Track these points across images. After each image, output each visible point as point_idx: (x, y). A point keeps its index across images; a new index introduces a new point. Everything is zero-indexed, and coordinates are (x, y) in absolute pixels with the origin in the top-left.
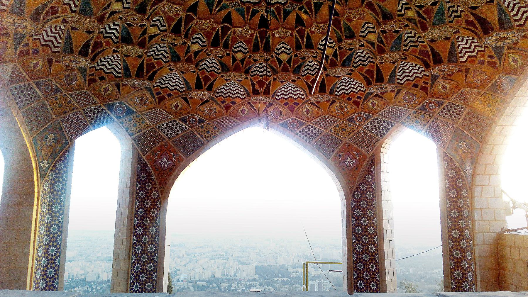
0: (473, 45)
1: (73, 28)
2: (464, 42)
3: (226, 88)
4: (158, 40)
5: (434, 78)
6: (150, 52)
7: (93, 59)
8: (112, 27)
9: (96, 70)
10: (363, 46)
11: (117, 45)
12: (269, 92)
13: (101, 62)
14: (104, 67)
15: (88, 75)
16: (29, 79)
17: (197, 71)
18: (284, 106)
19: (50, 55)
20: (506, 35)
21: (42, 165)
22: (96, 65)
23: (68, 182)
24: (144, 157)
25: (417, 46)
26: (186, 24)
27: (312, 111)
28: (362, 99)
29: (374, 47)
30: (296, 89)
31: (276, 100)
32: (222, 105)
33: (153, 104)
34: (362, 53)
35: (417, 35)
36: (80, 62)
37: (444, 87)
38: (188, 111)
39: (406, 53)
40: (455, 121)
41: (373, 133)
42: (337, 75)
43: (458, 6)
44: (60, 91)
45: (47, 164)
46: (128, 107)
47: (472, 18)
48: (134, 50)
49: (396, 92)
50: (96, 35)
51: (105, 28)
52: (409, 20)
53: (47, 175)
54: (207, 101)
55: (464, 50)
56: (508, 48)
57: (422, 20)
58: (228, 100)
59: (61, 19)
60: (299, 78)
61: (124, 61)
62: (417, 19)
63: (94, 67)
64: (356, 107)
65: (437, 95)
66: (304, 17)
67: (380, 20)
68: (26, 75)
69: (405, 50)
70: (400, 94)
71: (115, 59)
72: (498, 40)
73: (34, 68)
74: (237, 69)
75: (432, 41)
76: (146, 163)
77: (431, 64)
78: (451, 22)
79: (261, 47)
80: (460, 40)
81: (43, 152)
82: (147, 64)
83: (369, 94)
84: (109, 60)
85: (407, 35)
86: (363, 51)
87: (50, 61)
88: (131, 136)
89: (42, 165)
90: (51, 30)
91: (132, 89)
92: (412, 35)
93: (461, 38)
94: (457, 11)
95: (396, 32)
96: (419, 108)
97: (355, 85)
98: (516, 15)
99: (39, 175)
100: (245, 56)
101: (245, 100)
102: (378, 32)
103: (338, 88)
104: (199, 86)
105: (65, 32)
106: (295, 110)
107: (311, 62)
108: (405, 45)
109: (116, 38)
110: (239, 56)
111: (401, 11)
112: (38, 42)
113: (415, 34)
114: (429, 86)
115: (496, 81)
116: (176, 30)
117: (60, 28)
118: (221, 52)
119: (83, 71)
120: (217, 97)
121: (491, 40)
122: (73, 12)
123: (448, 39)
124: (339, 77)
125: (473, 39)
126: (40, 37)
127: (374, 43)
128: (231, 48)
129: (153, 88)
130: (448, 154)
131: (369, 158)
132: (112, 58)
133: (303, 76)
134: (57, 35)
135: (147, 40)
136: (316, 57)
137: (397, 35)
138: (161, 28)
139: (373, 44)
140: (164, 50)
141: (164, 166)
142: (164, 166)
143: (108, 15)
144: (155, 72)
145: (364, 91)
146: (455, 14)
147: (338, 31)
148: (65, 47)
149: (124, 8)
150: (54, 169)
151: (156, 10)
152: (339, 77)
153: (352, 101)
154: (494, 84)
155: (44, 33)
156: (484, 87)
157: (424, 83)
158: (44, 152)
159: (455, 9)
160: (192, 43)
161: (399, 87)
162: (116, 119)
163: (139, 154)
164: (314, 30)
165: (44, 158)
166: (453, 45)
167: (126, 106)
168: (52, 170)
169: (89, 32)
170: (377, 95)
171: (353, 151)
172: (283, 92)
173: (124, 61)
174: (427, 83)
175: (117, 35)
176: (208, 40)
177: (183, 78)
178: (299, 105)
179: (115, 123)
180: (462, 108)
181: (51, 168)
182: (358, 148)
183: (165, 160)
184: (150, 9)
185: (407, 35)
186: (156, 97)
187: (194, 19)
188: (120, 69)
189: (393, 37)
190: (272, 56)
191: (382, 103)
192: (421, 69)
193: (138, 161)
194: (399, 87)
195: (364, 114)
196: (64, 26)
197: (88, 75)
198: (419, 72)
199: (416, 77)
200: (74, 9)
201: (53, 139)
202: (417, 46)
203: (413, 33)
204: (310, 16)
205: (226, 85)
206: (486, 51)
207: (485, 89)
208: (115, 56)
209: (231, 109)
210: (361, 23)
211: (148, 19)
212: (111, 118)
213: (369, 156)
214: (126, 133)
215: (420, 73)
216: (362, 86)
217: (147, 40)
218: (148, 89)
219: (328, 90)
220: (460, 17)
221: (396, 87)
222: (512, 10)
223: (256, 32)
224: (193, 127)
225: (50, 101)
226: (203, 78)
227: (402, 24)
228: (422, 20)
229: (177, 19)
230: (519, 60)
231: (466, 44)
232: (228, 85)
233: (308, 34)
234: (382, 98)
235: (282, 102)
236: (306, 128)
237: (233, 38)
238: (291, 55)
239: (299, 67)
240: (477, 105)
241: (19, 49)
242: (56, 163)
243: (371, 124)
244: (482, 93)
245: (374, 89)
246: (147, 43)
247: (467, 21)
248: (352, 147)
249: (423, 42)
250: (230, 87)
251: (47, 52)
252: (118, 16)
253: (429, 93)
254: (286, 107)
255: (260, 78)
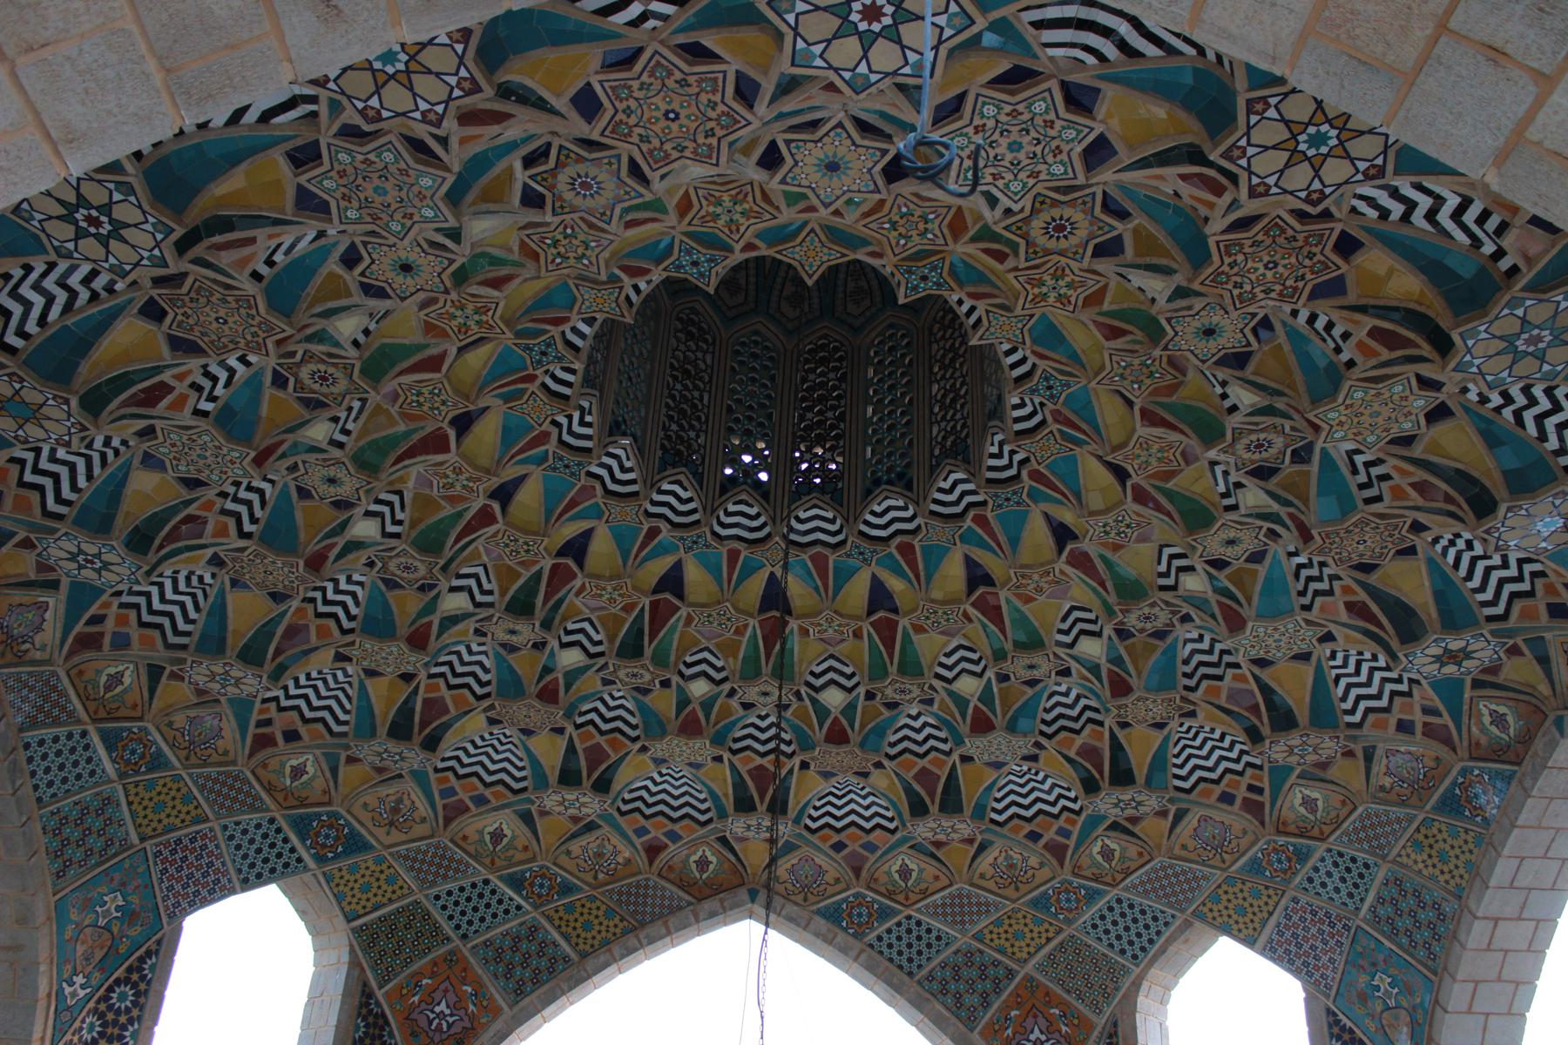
0: (1377, 676)
1: (234, 583)
2: (1351, 669)
3: (654, 789)
4: (466, 632)
5: (1280, 774)
6: (437, 665)
7: (276, 675)
8: (343, 586)
9: (281, 709)
10: (1066, 672)
11: (349, 638)
12: (785, 803)
13: (298, 686)
14: (302, 703)
15: (252, 723)
16: (85, 717)
17: (570, 729)
18: (831, 853)
19: (159, 654)
20: (1462, 644)
21: (68, 990)
22: (281, 693)
23: (154, 985)
24: (379, 994)
25: (1220, 678)
26: (552, 589)
27: (921, 871)
28: (1074, 836)
29: (1100, 679)
30: (871, 799)
31: (805, 833)
32: (638, 842)
33: (427, 825)
34: (1066, 694)
35: (1218, 647)
36: (238, 682)
37: (1309, 803)
38: (529, 855)
39: (1191, 696)
40: (1351, 907)
41: (1111, 946)
42: (993, 759)
43: (1322, 564)
44: (167, 765)
45: (83, 987)
46: (352, 829)
47: (1362, 596)
48: (394, 655)
49: (1171, 818)
50: (295, 604)
51: (324, 590)
52: (1190, 599)
53: (77, 1024)
54: (591, 827)
55: (1354, 692)
56: (1477, 684)
57: (1229, 602)
58: (658, 826)
59: (209, 552)
60: (879, 765)
61: (362, 687)
62: (1213, 598)
63: (276, 699)
64: (1055, 862)
65: (1292, 828)
66: (895, 584)
67: (1112, 599)
68: (79, 707)
69: (1186, 688)
70: (1184, 823)
71: (337, 682)
72: (1440, 660)
73: (108, 688)
74: (690, 728)
75: (1261, 663)
76: (383, 1015)
77: (1266, 730)
78: (1307, 608)
79: (766, 669)
80: (1339, 662)
81: (80, 949)
82: (425, 701)
83: (1095, 820)
84: (320, 684)
85: (1189, 647)
86: (1069, 690)
87: (155, 673)
88: (349, 921)
89: (68, 990)
90: (175, 582)
91: (372, 773)
92: (1205, 645)
93: (1340, 656)
94: (1320, 579)
95: (1160, 635)
96: (1242, 868)
97: (1049, 792)
98: (1482, 588)
99: (51, 1022)
100: (717, 689)
101: (712, 826)
102: (1108, 631)
103: (998, 800)
104: (569, 777)
105: (212, 593)
106: (867, 866)
107: (915, 718)
108: (1185, 675)
109: (351, 618)
110: (699, 688)
111: (1166, 575)
112: (133, 614)
113: (1213, 641)
114: (1266, 798)
115: (1454, 783)
116: (521, 607)
117: (201, 578)
118: (647, 677)
119: (242, 707)
120: (622, 814)
121: (1423, 660)
122: (243, 535)
123: (1304, 657)
124: (1003, 764)
125: (1375, 658)
126: (142, 600)
127: (1098, 666)
128: (676, 664)
129: (432, 776)
130: (1341, 1016)
131: (1099, 1029)
132: (330, 679)
133: (891, 758)
134: (188, 600)
135: (435, 628)
136: (930, 702)
137: (1162, 645)
138: (479, 598)
139: (1095, 669)
140: (480, 663)
141: (439, 1028)
142: (439, 1028)
143: (336, 551)
144: (446, 727)
145: (1078, 813)
146: (1314, 586)
147: (993, 627)
148: (204, 637)
149: (385, 534)
150: (102, 1007)
151: (471, 547)
152: (1003, 764)
153: (1042, 842)
154: (1450, 790)
155: (154, 590)
156: (1423, 800)
157: (1251, 788)
158: (85, 947)
159: (1315, 572)
160: (564, 646)
161: (1180, 800)
162: (312, 864)
163: (365, 984)
164: (922, 622)
165: (79, 968)
166: (1319, 670)
167: (348, 824)
168: (95, 1011)
169: (277, 597)
170: (1115, 826)
171: (1049, 1004)
172: (829, 808)
173: (362, 687)
174: (1260, 791)
175: (354, 610)
176: (611, 640)
177: (527, 750)
178: (879, 853)
179: (307, 877)
180: (1367, 866)
181: (91, 1004)
182: (1065, 995)
183: (443, 1006)
184: (457, 541)
185: (1189, 647)
186: (439, 803)
187: (574, 576)
188: (346, 712)
189: (1151, 649)
190: (798, 694)
191: (1132, 851)
192: (1238, 747)
193: (361, 1006)
194: (1180, 800)
195: (1080, 886)
196: (213, 576)
197: (252, 723)
198: (1234, 755)
199: (1227, 771)
200: (248, 527)
201: (118, 908)
202: (1220, 678)
203: (1207, 639)
204: (910, 582)
205: (652, 779)
206: (1415, 692)
207: (1428, 807)
208: (340, 674)
209: (663, 857)
210: (1060, 608)
211: (444, 569)
212: (299, 860)
213: (1100, 1021)
214: (337, 911)
215: (1237, 761)
216: (1072, 795)
217: (435, 628)
218: (420, 777)
219: (969, 802)
220: (1330, 592)
221: (1171, 800)
222: (1469, 577)
223: (752, 622)
224: (541, 905)
225: (133, 791)
226: (585, 750)
227: (1174, 613)
228: (1229, 602)
229: (526, 575)
230: (1510, 719)
231: (1357, 673)
232: (659, 780)
233: (906, 634)
234: (1133, 834)
235: (824, 839)
236: (899, 924)
237: (682, 635)
238: (854, 693)
239: (880, 732)
240: (1408, 856)
241: (79, 627)
242: (110, 989)
243: (1103, 918)
244: (1420, 818)
245: (1108, 803)
246: (433, 638)
247: (1350, 606)
248: (1047, 994)
249: (1237, 666)
250: (666, 786)
251: (153, 647)
252: (362, 556)
253: (1267, 819)
254: (838, 857)
255: (759, 761)
